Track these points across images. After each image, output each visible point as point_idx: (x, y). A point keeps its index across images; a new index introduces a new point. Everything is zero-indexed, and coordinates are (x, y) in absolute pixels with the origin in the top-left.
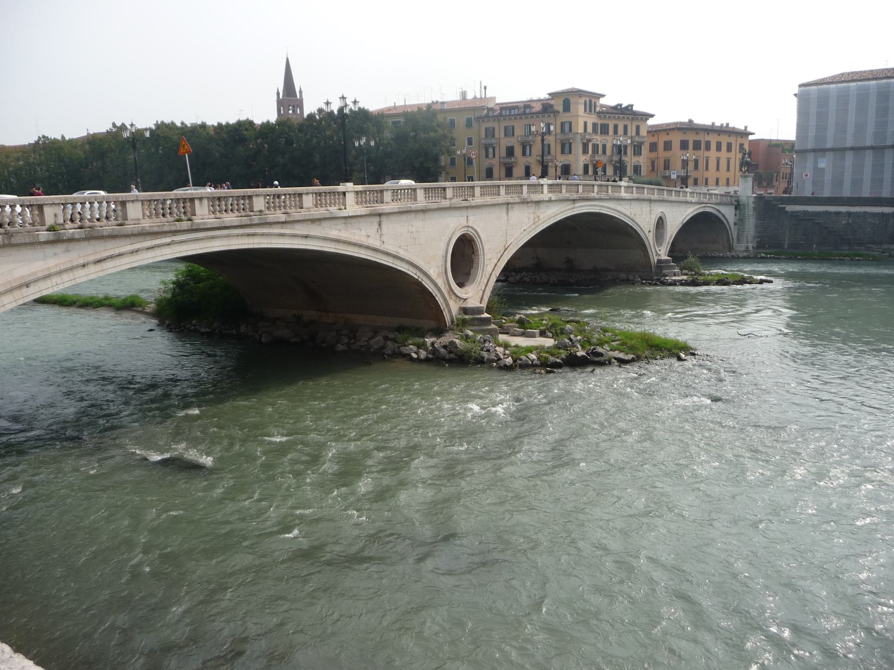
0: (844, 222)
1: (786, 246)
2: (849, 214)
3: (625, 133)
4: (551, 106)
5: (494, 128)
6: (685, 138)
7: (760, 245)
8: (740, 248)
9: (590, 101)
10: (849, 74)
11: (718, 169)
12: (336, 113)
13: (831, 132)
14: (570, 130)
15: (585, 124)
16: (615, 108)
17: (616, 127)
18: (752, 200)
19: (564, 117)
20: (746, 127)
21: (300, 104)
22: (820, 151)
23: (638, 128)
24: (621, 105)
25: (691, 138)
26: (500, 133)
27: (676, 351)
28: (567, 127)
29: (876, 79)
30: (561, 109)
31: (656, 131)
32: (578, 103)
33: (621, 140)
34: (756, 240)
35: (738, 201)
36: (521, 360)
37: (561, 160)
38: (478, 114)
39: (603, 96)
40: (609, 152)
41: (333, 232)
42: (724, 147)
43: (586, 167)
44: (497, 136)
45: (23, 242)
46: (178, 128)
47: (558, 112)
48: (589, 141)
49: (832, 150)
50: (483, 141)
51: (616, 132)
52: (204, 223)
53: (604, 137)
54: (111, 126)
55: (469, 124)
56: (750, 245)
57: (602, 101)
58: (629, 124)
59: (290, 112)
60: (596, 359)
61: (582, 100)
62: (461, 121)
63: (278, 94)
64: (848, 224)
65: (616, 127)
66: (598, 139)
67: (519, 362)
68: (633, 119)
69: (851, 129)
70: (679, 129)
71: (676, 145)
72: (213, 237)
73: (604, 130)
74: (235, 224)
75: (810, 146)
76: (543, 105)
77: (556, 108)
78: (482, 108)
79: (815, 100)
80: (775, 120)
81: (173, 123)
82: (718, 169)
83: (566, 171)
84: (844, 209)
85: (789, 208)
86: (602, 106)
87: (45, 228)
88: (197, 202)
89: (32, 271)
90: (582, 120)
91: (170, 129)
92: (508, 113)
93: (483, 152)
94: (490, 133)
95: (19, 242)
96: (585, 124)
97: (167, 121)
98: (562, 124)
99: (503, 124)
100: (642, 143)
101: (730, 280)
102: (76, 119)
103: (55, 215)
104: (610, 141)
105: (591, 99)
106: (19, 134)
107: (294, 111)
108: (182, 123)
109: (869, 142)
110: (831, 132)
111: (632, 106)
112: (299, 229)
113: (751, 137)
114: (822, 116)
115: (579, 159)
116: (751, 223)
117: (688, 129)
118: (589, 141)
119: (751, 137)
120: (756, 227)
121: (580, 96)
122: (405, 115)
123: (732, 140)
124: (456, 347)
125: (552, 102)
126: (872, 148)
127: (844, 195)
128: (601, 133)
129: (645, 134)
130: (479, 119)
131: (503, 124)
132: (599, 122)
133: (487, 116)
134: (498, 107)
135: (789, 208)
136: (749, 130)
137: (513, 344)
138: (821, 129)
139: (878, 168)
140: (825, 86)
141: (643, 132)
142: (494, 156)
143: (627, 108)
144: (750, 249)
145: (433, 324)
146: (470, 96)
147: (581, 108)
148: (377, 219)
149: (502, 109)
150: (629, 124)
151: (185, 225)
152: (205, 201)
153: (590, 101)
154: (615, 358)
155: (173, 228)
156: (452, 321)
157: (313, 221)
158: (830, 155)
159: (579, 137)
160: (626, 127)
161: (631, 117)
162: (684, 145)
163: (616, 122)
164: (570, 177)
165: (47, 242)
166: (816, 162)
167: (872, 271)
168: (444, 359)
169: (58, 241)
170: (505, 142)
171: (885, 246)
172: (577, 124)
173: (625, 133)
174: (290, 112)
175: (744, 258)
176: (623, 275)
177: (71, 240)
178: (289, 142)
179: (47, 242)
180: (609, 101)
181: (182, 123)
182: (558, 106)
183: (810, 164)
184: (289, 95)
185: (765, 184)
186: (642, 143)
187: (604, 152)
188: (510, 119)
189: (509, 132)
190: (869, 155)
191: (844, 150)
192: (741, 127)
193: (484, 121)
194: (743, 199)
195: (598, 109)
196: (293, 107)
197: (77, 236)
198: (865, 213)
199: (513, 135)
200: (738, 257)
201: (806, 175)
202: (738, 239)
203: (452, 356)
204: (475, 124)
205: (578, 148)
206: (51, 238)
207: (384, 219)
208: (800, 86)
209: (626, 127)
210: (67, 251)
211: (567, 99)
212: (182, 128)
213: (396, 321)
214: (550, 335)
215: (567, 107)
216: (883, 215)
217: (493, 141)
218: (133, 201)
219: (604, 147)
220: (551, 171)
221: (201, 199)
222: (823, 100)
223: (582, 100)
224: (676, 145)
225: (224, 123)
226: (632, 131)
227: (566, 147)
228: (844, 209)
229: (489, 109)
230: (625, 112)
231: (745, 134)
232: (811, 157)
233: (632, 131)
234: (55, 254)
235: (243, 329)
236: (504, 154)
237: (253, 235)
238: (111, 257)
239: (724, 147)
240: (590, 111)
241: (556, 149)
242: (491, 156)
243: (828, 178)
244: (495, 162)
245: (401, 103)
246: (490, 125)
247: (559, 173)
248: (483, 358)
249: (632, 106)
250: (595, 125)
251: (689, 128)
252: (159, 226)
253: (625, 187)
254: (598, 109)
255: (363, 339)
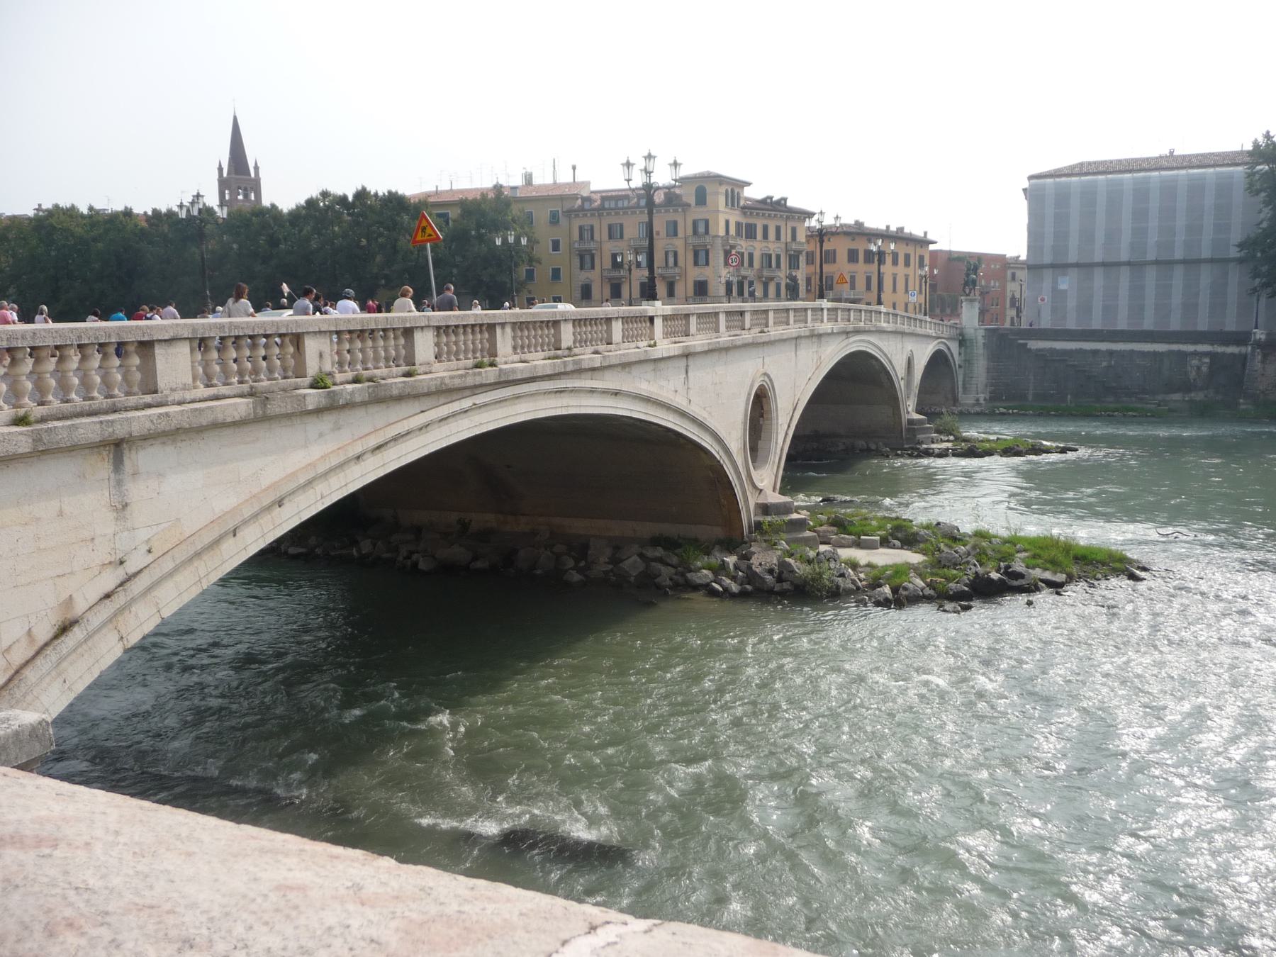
0: (1104, 364)
1: (1030, 397)
2: (1111, 353)
3: (778, 238)
4: (678, 197)
5: (592, 227)
6: (853, 246)
7: (994, 397)
8: (967, 400)
9: (733, 191)
10: (1090, 163)
11: (894, 290)
12: (350, 198)
13: (1073, 242)
14: (707, 232)
15: (727, 222)
16: (763, 201)
17: (765, 228)
18: (981, 333)
19: (698, 213)
20: (926, 233)
21: (255, 185)
22: (1060, 267)
23: (794, 230)
24: (771, 198)
25: (861, 246)
26: (601, 234)
27: (1121, 566)
28: (702, 228)
29: (1130, 171)
30: (692, 201)
31: (822, 235)
32: (717, 193)
33: (773, 247)
34: (988, 390)
35: (961, 334)
36: (906, 589)
37: (695, 274)
38: (567, 206)
39: (749, 184)
40: (756, 264)
41: (644, 384)
42: (901, 260)
43: (729, 285)
44: (597, 236)
45: (283, 411)
46: (82, 216)
47: (689, 205)
48: (733, 247)
49: (1077, 265)
50: (576, 245)
51: (765, 236)
52: (514, 371)
53: (750, 243)
54: (1261, 140)
55: (554, 220)
56: (982, 396)
57: (748, 193)
58: (782, 224)
59: (240, 197)
60: (1015, 583)
61: (722, 189)
62: (542, 216)
63: (220, 169)
64: (1109, 366)
65: (765, 228)
66: (743, 245)
67: (902, 592)
68: (788, 218)
69: (1100, 237)
70: (847, 234)
71: (842, 256)
72: (518, 397)
73: (750, 232)
74: (549, 372)
75: (1047, 259)
76: (665, 194)
77: (685, 199)
78: (574, 197)
79: (1056, 200)
80: (995, 227)
81: (73, 207)
82: (894, 290)
83: (701, 290)
84: (1103, 346)
85: (1034, 345)
86: (747, 199)
87: (308, 380)
88: (499, 330)
89: (289, 471)
90: (724, 219)
91: (71, 216)
92: (613, 205)
93: (577, 261)
94: (587, 233)
95: (278, 411)
96: (727, 222)
97: (64, 203)
98: (695, 223)
99: (606, 222)
100: (800, 252)
101: (1021, 448)
102: (153, 172)
103: (321, 355)
104: (758, 247)
105: (734, 187)
106: (15, 197)
107: (246, 196)
108: (91, 208)
109: (1124, 257)
110: (1073, 242)
111: (785, 200)
112: (610, 381)
113: (932, 247)
114: (1061, 219)
115: (719, 273)
116: (981, 367)
117: (858, 234)
118: (733, 247)
119: (932, 247)
120: (988, 370)
121: (721, 184)
122: (463, 204)
123: (910, 249)
124: (793, 571)
125: (677, 191)
126: (1129, 263)
127: (1119, 328)
128: (747, 237)
129: (804, 240)
130: (570, 213)
131: (606, 222)
132: (744, 221)
133: (582, 209)
134: (597, 197)
135: (1034, 345)
136: (930, 237)
137: (863, 562)
138: (1061, 235)
139: (1137, 291)
140: (1063, 179)
141: (801, 237)
142: (593, 267)
143: (778, 202)
144: (982, 401)
145: (718, 532)
146: (537, 181)
147: (722, 200)
148: (683, 362)
149: (604, 199)
150: (782, 224)
151: (489, 374)
152: (508, 330)
153: (733, 191)
154: (1042, 581)
155: (470, 381)
156: (750, 527)
157: (626, 366)
158: (1074, 273)
159: (719, 241)
160: (778, 229)
161: (785, 215)
162: (853, 256)
163: (765, 222)
164: (708, 300)
165: (318, 411)
166: (1055, 283)
167: (1109, 430)
168: (771, 592)
169: (333, 407)
170: (609, 247)
171: (1160, 397)
172: (717, 224)
173: (778, 238)
174: (240, 197)
175: (977, 414)
176: (861, 443)
177: (350, 405)
178: (273, 242)
179: (318, 411)
180: (753, 193)
181: (91, 208)
182: (689, 196)
183: (1047, 284)
184: (238, 173)
185: (948, 311)
186: (800, 252)
187: (751, 264)
188: (617, 214)
189: (615, 232)
190: (1125, 273)
191: (1092, 265)
192: (919, 233)
193: (577, 216)
194: (969, 332)
195: (742, 203)
196: (245, 189)
197: (358, 399)
198: (1132, 351)
199: (622, 237)
200: (970, 414)
201: (1043, 300)
202: (965, 388)
203: (786, 586)
204: (563, 221)
205: (717, 257)
206: (324, 402)
207: (690, 359)
208: (1031, 178)
209: (778, 229)
210: (337, 428)
211: (703, 187)
212: (90, 217)
213: (648, 529)
214: (897, 543)
215: (701, 198)
216: (1155, 353)
217: (592, 245)
218: (422, 328)
219: (751, 256)
220: (679, 289)
221: (503, 325)
222: (1062, 197)
223: (722, 189)
224: (842, 256)
225: (164, 210)
226: (786, 236)
227: (701, 256)
228: (1103, 346)
229: (585, 199)
230: (774, 208)
231: (924, 242)
232: (1048, 275)
233: (786, 236)
234: (321, 435)
235: (366, 546)
236: (608, 264)
237: (560, 391)
238: (396, 439)
239: (901, 260)
240: (733, 205)
241: (686, 259)
242: (588, 265)
243: (1071, 303)
244: (594, 276)
245: (444, 186)
246: (586, 222)
247: (691, 292)
248: (838, 587)
249: (785, 200)
250: (738, 225)
251: (858, 232)
252: (461, 376)
253: (666, 318)
254: (742, 203)
255: (602, 560)
